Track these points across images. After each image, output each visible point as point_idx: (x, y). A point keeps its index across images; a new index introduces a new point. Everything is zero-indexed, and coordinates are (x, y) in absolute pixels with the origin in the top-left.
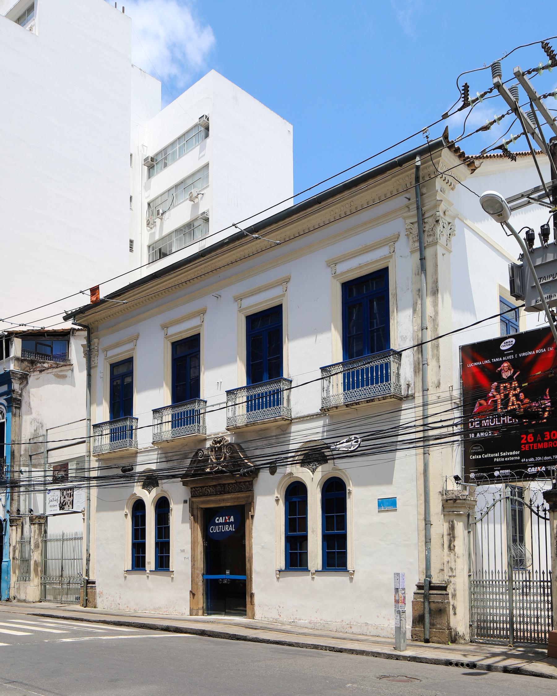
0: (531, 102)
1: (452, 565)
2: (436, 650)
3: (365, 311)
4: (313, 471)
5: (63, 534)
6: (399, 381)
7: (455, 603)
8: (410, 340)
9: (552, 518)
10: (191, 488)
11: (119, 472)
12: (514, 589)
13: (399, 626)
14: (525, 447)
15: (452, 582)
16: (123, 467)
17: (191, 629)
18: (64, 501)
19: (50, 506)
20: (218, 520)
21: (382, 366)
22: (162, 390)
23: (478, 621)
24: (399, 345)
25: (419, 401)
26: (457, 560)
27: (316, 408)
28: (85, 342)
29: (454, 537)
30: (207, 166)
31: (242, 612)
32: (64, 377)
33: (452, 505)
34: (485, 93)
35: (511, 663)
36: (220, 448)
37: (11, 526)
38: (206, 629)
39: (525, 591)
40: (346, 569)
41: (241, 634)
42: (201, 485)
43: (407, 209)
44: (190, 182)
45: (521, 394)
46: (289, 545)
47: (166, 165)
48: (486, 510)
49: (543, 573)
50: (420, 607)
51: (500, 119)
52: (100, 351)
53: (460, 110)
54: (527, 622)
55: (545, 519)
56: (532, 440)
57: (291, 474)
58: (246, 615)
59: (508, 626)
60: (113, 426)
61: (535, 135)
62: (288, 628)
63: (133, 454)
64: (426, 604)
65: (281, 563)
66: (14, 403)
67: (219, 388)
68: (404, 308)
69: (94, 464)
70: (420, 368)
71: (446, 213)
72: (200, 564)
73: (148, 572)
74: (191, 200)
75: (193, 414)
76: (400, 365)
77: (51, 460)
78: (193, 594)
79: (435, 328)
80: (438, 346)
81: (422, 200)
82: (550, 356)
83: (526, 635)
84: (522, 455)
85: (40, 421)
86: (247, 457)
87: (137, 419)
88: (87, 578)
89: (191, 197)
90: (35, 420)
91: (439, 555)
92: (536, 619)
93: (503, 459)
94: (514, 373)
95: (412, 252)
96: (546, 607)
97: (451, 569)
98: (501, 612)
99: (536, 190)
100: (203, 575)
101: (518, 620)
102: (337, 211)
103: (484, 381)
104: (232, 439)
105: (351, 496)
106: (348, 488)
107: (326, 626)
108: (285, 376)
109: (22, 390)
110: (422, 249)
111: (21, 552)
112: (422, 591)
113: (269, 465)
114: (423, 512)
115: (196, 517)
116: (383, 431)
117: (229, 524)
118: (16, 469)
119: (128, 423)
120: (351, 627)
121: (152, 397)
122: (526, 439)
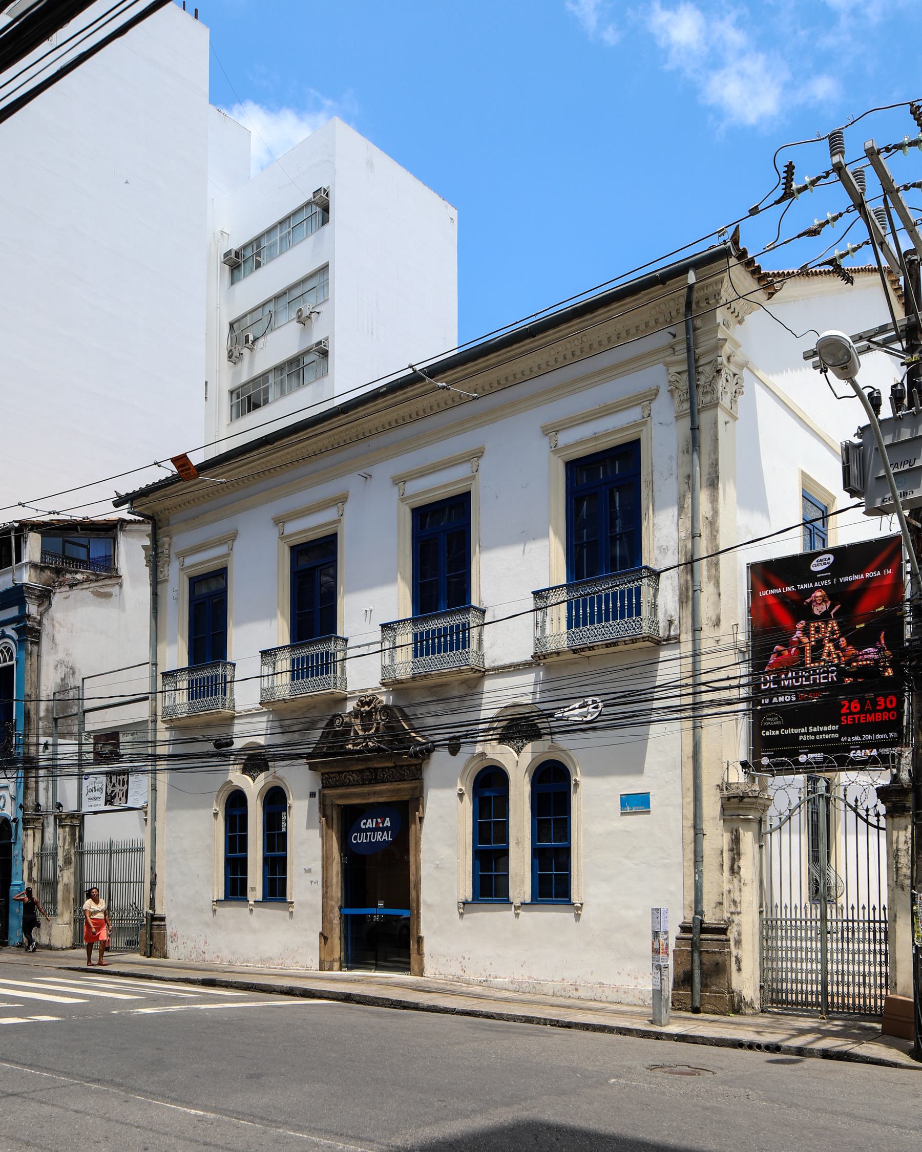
0: (885, 195)
1: (736, 896)
2: (713, 1024)
3: (603, 510)
4: (518, 751)
5: (111, 843)
6: (655, 615)
7: (740, 953)
8: (674, 554)
9: (890, 827)
10: (323, 774)
11: (210, 747)
12: (829, 933)
13: (659, 988)
14: (846, 719)
15: (736, 922)
16: (217, 740)
17: (329, 992)
18: (113, 791)
19: (90, 799)
20: (365, 824)
21: (630, 591)
22: (274, 623)
23: (773, 980)
24: (656, 560)
25: (686, 648)
26: (744, 888)
27: (525, 653)
28: (147, 542)
29: (739, 854)
30: (325, 268)
31: (405, 967)
32: (108, 595)
33: (739, 808)
34: (818, 179)
35: (828, 1043)
36: (369, 713)
37: (25, 829)
38: (354, 992)
39: (845, 936)
40: (570, 900)
41: (409, 1000)
42: (338, 770)
43: (671, 351)
44: (296, 293)
45: (841, 639)
46: (478, 862)
47: (258, 265)
48: (787, 813)
49: (874, 909)
50: (685, 958)
51: (835, 219)
52: (173, 556)
53: (778, 202)
54: (848, 982)
55: (878, 828)
56: (858, 709)
57: (483, 754)
58: (409, 970)
59: (820, 989)
60: (196, 676)
61: (884, 245)
62: (478, 990)
63: (226, 719)
64: (696, 955)
65: (467, 892)
66: (30, 634)
67: (368, 619)
68: (665, 506)
69: (163, 735)
70: (689, 596)
71: (732, 359)
72: (336, 891)
73: (251, 902)
74: (299, 322)
75: (327, 660)
76: (657, 590)
77: (88, 727)
78: (324, 937)
79: (714, 536)
80: (717, 564)
81: (695, 339)
82: (887, 582)
83: (846, 1002)
84: (842, 732)
85: (70, 665)
86: (414, 729)
87: (234, 665)
88: (151, 912)
89: (299, 317)
90: (61, 662)
91: (715, 881)
92: (861, 978)
93: (813, 738)
94: (831, 608)
95: (678, 418)
96: (878, 960)
97: (734, 902)
98: (809, 967)
99: (883, 329)
100: (340, 908)
101: (835, 979)
102: (560, 349)
103: (784, 618)
104: (388, 699)
105: (579, 790)
106: (573, 778)
107: (538, 987)
108: (474, 602)
109: (41, 615)
110: (693, 414)
111: (41, 870)
112: (690, 936)
113: (447, 742)
114: (691, 816)
115: (330, 819)
116: (638, 691)
117: (383, 830)
118: (33, 740)
119: (220, 671)
120: (576, 990)
121: (257, 632)
122: (849, 708)
